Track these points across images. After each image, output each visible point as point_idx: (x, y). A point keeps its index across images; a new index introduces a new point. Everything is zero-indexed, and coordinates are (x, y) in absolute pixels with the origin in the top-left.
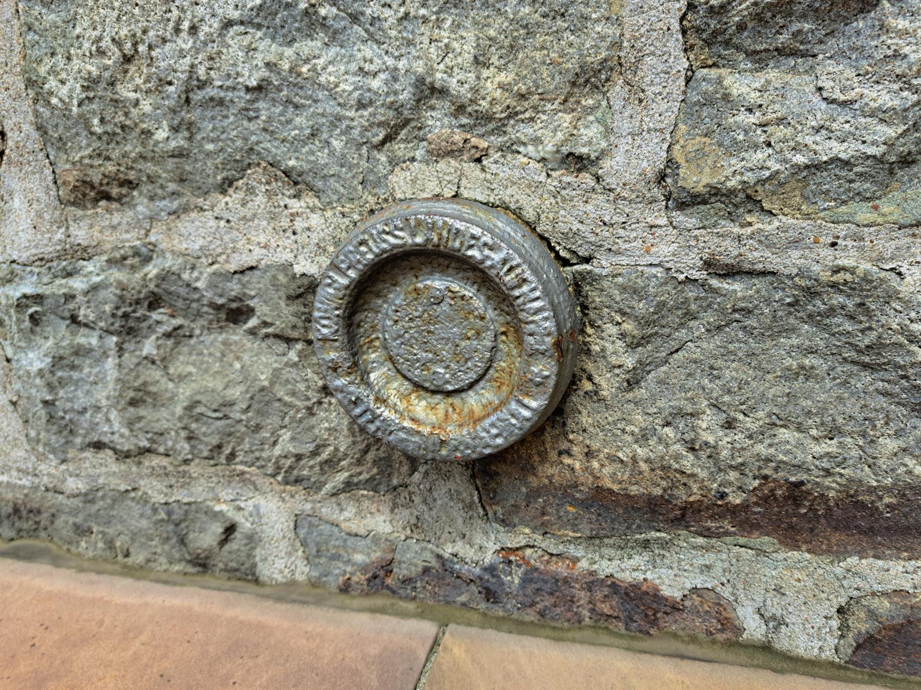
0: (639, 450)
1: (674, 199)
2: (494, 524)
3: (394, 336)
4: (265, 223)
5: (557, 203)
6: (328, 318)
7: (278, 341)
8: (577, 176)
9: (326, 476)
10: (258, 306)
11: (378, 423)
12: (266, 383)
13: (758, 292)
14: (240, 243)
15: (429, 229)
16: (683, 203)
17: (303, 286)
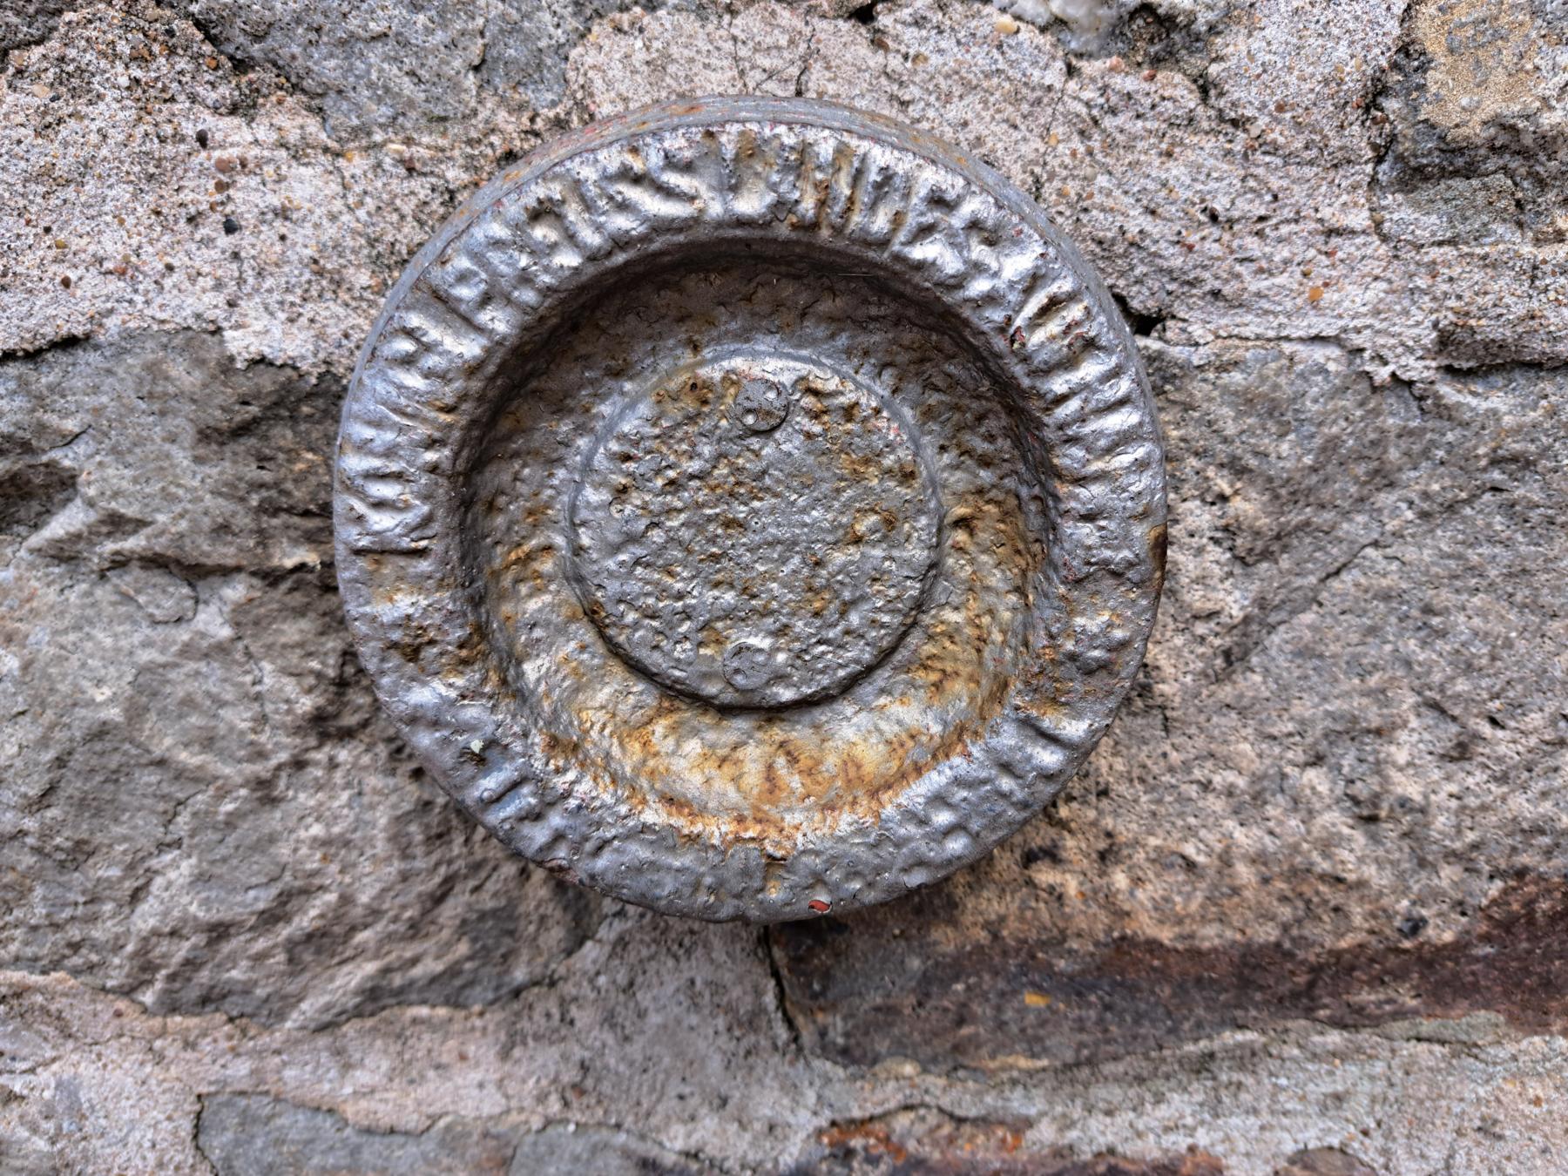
0: (1239, 834)
1: (1400, 158)
2: (817, 1063)
3: (613, 537)
4: (123, 192)
5: (1090, 153)
6: (398, 477)
7: (158, 578)
8: (1152, 78)
9: (307, 975)
10: (90, 466)
11: (556, 820)
12: (114, 714)
13: (1553, 413)
14: (30, 259)
15: (787, 168)
16: (1419, 169)
17: (257, 396)
